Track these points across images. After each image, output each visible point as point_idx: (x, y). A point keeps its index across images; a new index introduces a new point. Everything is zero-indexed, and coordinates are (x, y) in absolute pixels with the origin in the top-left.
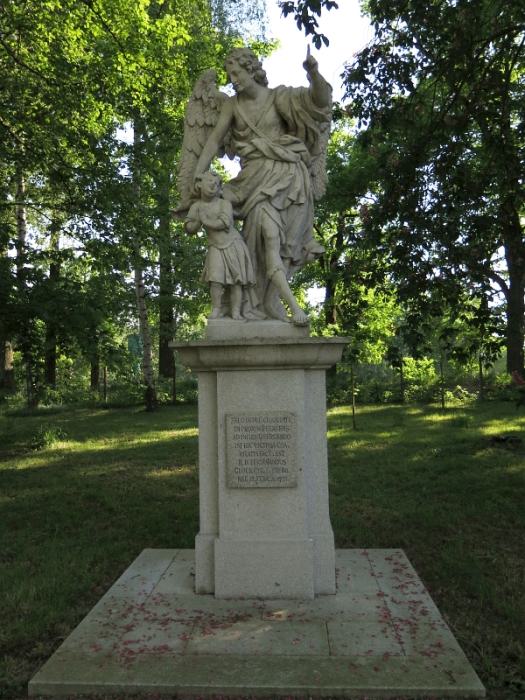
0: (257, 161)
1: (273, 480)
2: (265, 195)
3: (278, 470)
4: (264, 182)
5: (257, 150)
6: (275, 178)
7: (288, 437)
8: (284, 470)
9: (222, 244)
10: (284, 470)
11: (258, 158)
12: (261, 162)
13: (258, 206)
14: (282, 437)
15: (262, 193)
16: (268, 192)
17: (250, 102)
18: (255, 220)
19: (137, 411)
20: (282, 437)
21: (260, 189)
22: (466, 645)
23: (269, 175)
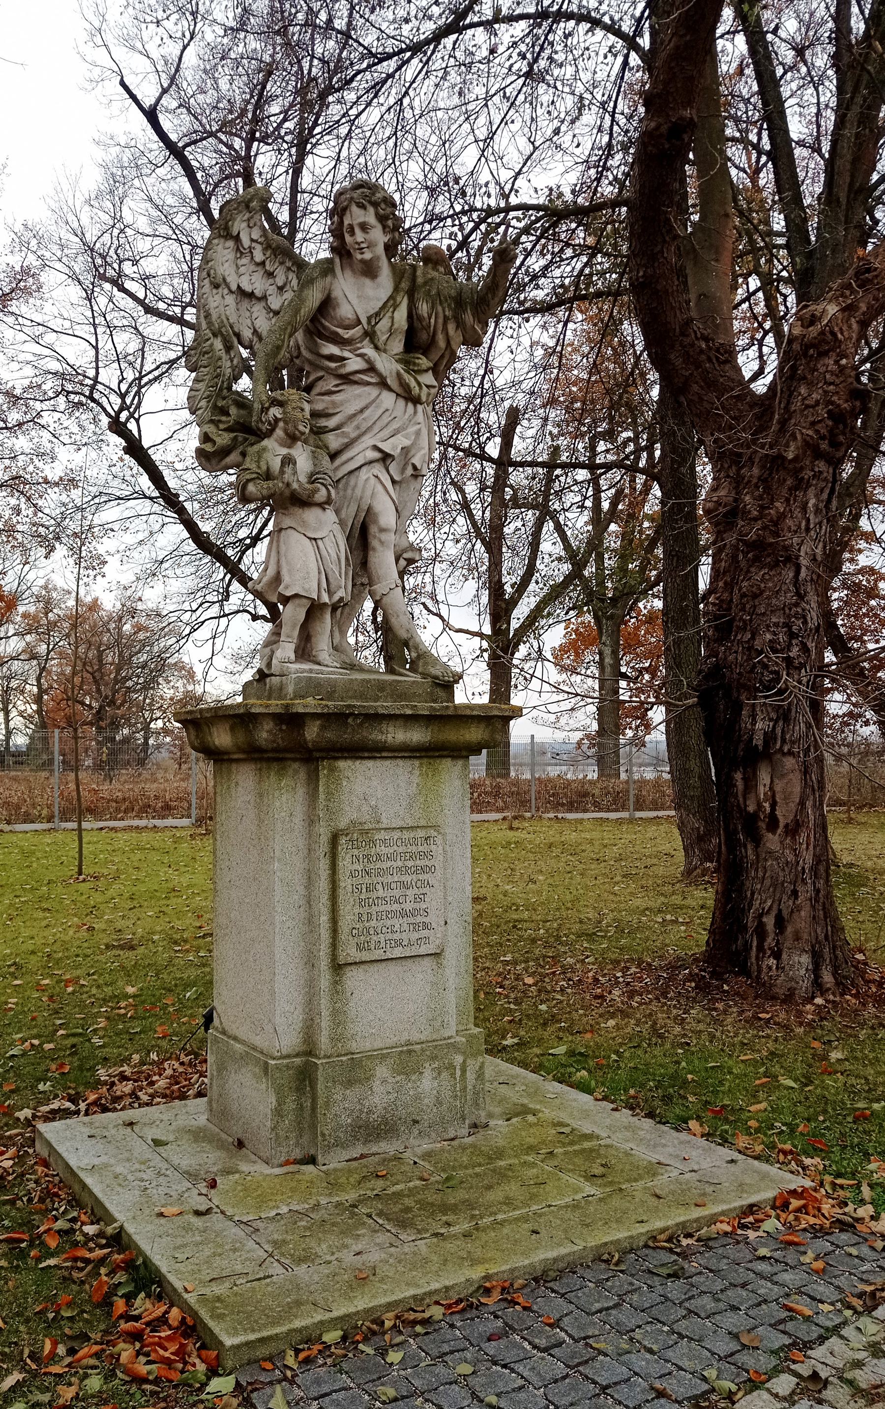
0: (367, 389)
1: (410, 944)
2: (380, 450)
3: (415, 927)
4: (376, 429)
5: (371, 369)
6: (395, 425)
7: (431, 869)
8: (426, 926)
9: (315, 530)
10: (426, 926)
11: (368, 384)
12: (374, 392)
13: (364, 469)
14: (423, 870)
15: (376, 448)
16: (386, 447)
17: (368, 281)
18: (358, 492)
19: (819, 930)
20: (423, 870)
21: (368, 441)
22: (75, 1202)
23: (386, 419)
